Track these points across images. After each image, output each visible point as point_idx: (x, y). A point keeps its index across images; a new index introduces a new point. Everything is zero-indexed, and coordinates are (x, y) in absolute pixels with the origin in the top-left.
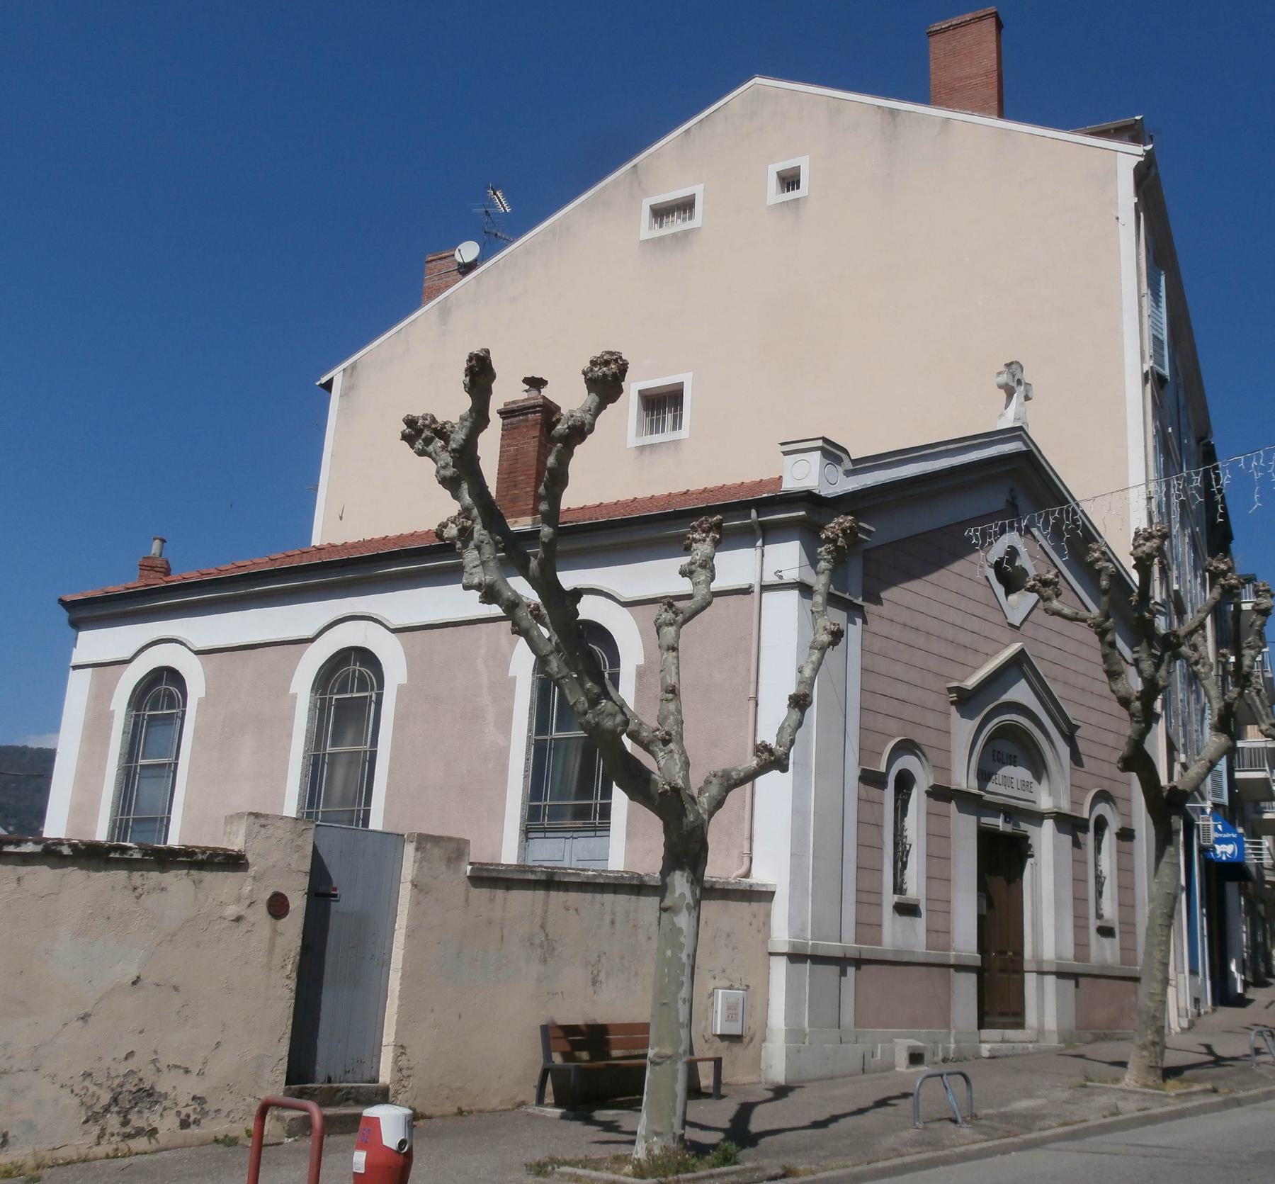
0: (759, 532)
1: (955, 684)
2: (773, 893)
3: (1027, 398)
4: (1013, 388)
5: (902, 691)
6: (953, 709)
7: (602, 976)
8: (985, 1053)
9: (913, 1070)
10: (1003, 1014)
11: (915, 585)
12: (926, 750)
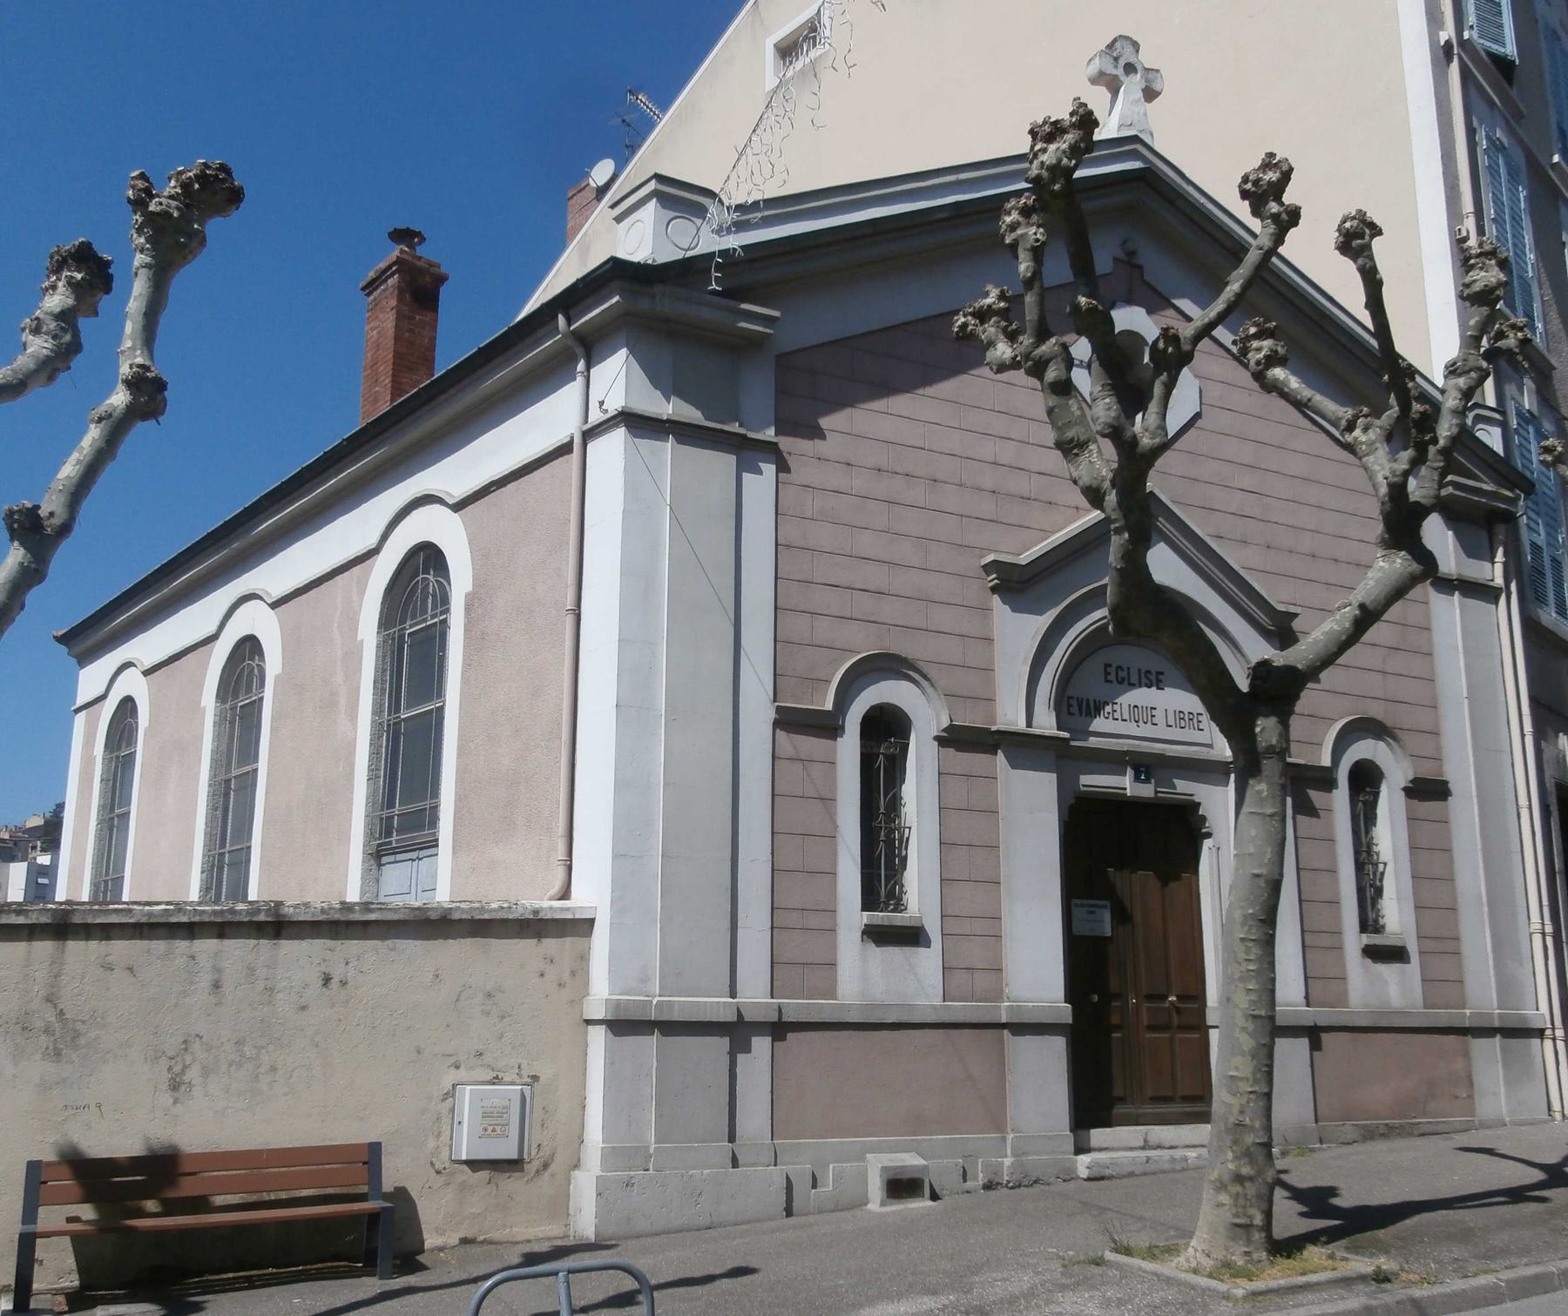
0: (580, 351)
1: (990, 558)
2: (592, 921)
3: (1150, 94)
4: (1116, 77)
5: (875, 577)
6: (996, 600)
7: (193, 1075)
8: (1083, 1172)
9: (897, 1207)
10: (1156, 1099)
11: (900, 403)
12: (932, 672)
